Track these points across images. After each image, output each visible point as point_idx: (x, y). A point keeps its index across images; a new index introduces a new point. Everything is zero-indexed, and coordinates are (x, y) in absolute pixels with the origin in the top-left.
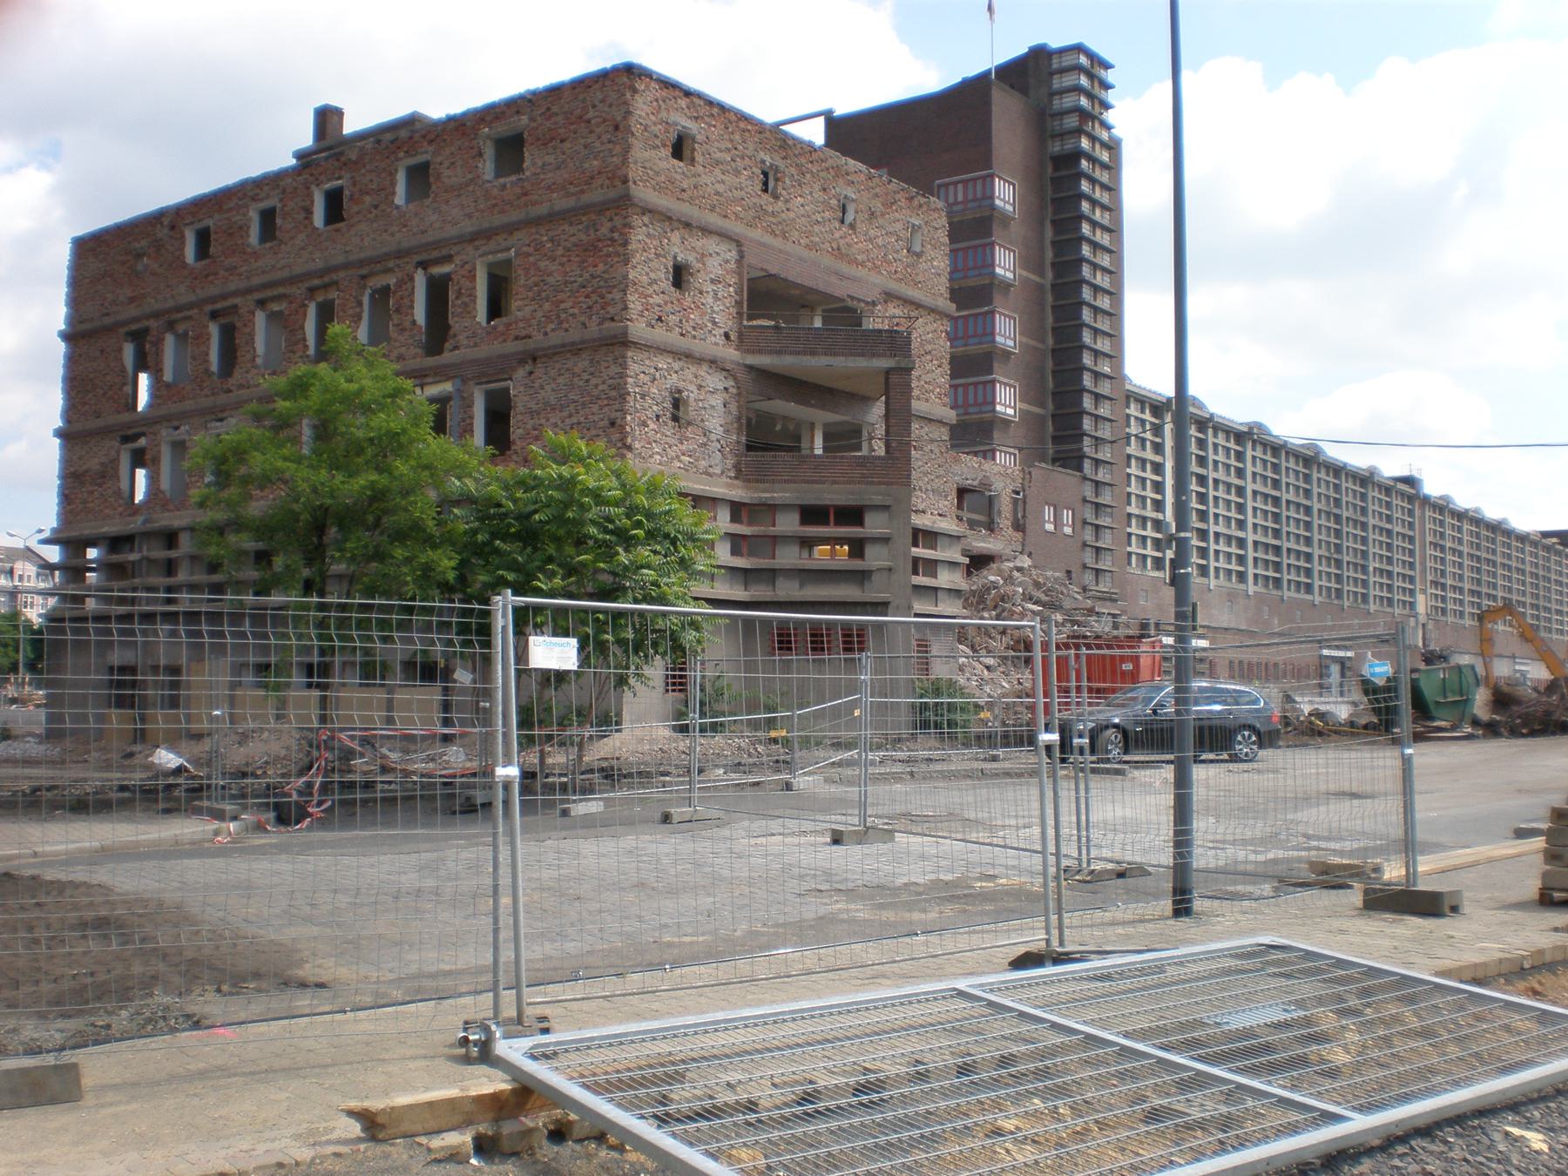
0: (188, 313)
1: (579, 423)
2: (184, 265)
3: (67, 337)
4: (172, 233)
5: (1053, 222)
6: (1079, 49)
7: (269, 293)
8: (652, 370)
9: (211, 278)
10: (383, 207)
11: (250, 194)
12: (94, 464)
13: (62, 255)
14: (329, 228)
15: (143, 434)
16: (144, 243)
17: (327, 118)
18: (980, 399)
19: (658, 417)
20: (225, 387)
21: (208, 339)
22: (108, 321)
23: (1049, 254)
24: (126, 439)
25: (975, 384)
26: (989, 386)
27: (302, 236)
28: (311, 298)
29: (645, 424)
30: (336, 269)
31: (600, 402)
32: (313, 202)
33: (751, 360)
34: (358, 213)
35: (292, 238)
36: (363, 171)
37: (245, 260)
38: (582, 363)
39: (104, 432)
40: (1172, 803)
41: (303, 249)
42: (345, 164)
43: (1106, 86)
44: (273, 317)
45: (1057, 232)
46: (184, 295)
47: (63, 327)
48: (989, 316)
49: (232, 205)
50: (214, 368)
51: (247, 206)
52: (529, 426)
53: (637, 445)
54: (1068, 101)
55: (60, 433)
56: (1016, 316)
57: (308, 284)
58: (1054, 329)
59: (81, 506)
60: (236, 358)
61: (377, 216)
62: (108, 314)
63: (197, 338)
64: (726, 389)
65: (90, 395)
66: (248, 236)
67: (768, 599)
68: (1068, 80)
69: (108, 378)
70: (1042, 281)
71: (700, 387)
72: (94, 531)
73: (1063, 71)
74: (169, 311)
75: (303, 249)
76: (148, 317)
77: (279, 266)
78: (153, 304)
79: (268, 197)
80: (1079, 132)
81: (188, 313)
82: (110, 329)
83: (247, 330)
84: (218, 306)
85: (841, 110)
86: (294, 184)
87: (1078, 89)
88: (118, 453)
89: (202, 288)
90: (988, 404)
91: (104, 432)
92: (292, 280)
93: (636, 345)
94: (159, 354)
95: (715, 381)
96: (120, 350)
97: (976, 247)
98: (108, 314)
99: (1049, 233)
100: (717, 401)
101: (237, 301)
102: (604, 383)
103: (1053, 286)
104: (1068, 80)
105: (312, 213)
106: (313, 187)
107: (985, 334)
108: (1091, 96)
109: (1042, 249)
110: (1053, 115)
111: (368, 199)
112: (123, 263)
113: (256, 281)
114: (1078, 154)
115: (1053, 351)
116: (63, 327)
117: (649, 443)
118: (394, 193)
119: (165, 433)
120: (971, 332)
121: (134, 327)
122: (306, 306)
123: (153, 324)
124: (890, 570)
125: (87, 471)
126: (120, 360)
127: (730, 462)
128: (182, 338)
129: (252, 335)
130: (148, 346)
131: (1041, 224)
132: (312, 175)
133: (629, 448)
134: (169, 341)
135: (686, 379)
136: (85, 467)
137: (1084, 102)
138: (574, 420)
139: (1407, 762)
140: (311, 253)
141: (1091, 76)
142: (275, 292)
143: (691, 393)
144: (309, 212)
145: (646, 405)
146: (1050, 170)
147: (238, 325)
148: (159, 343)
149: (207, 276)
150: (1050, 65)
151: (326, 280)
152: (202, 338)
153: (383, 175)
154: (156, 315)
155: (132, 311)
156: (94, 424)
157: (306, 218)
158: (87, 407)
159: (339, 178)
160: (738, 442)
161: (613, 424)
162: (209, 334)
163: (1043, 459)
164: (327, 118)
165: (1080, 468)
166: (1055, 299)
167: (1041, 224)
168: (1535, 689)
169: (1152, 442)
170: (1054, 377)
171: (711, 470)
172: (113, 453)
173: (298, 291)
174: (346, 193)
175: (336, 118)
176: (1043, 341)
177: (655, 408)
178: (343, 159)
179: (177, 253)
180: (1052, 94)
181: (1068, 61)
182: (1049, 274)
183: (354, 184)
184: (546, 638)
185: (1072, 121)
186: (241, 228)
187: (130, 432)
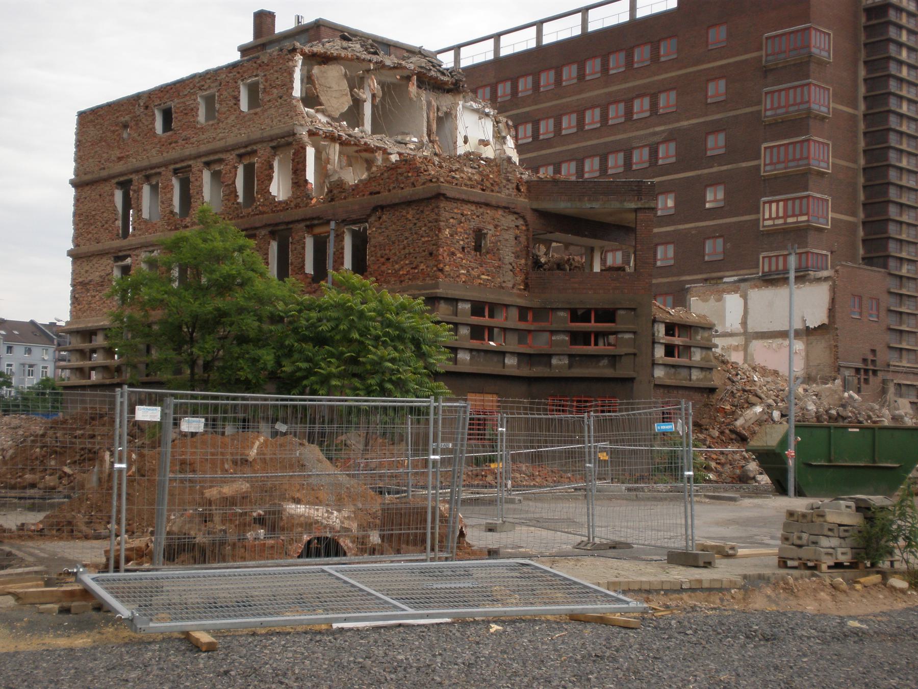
0: (158, 170)
1: (410, 254)
2: (155, 135)
3: (75, 184)
4: (146, 112)
5: (865, 63)
7: (212, 158)
8: (459, 216)
9: (173, 145)
10: (285, 97)
11: (198, 85)
12: (95, 276)
13: (74, 119)
14: (252, 111)
15: (129, 256)
16: (127, 118)
17: (263, 20)
19: (463, 248)
20: (184, 223)
21: (172, 189)
22: (104, 174)
23: (862, 90)
24: (118, 259)
25: (794, 199)
27: (233, 117)
28: (240, 162)
29: (453, 254)
30: (256, 142)
31: (423, 239)
32: (239, 92)
33: (536, 205)
34: (269, 101)
35: (227, 118)
36: (272, 71)
37: (196, 134)
38: (411, 214)
39: (102, 254)
41: (233, 126)
42: (260, 66)
44: (216, 175)
45: (869, 71)
46: (154, 156)
47: (73, 177)
48: (805, 144)
49: (186, 93)
50: (177, 210)
51: (195, 94)
52: (379, 255)
53: (447, 268)
55: (70, 254)
56: (830, 143)
57: (238, 152)
58: (865, 151)
59: (87, 306)
60: (191, 203)
61: (281, 104)
62: (104, 169)
63: (164, 188)
64: (517, 226)
65: (93, 227)
66: (197, 116)
67: (546, 375)
69: (105, 215)
70: (856, 112)
71: (496, 226)
72: (96, 324)
74: (146, 169)
75: (233, 126)
76: (131, 173)
77: (218, 138)
78: (134, 163)
79: (209, 87)
81: (158, 170)
82: (106, 180)
83: (198, 184)
84: (178, 166)
86: (227, 79)
88: (112, 268)
89: (168, 152)
91: (102, 254)
92: (226, 150)
93: (447, 198)
94: (139, 198)
95: (509, 221)
96: (113, 195)
97: (795, 87)
98: (104, 169)
99: (862, 73)
100: (510, 236)
101: (190, 163)
102: (425, 225)
103: (865, 116)
105: (239, 100)
106: (240, 82)
109: (856, 86)
111: (275, 91)
112: (114, 132)
113: (203, 148)
115: (864, 169)
116: (73, 177)
117: (457, 267)
118: (292, 88)
119: (144, 255)
120: (791, 157)
121: (122, 179)
122: (236, 168)
123: (134, 177)
124: (635, 354)
125: (91, 281)
126: (112, 202)
127: (519, 278)
128: (154, 189)
129: (201, 186)
130: (131, 193)
131: (855, 63)
132: (239, 73)
133: (441, 270)
134: (146, 189)
135: (488, 220)
136: (90, 278)
138: (407, 251)
140: (239, 129)
142: (216, 157)
143: (490, 230)
144: (237, 99)
145: (455, 241)
147: (192, 179)
148: (139, 191)
149: (170, 144)
151: (249, 149)
152: (169, 188)
153: (285, 74)
154: (137, 171)
155: (119, 167)
156: (95, 247)
157: (235, 104)
158: (90, 236)
159: (256, 76)
160: (526, 264)
161: (431, 254)
162: (172, 185)
163: (853, 259)
164: (263, 20)
165: (885, 266)
166: (867, 126)
167: (855, 63)
170: (864, 191)
171: (504, 285)
172: (109, 268)
173: (231, 157)
174: (261, 86)
175: (269, 20)
176: (855, 161)
177: (461, 243)
178: (259, 62)
179: (151, 126)
182: (862, 107)
183: (266, 81)
184: (144, 407)
186: (192, 109)
187: (120, 254)
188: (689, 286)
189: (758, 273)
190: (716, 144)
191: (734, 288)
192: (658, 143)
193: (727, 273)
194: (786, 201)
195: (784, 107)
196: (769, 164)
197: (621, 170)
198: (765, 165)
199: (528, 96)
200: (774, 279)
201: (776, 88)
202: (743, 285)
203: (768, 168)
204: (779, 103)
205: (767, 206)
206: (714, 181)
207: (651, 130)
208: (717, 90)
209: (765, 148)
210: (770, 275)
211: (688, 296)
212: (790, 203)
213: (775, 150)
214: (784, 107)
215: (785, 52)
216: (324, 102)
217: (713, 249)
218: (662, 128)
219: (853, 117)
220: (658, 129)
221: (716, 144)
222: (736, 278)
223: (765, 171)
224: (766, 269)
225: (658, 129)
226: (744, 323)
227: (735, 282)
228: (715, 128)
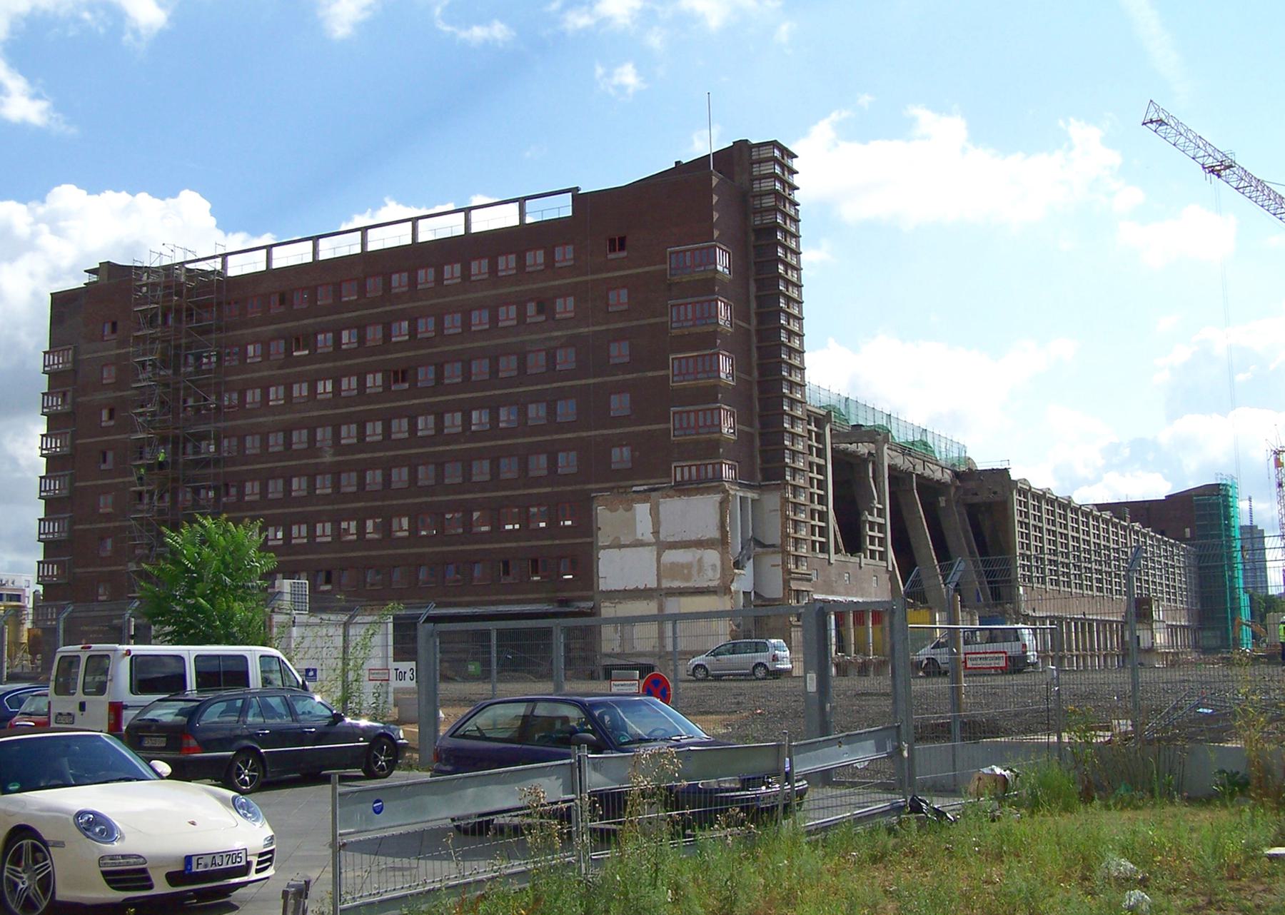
5: (756, 280)
6: (775, 144)
18: (709, 422)
23: (753, 305)
25: (704, 411)
26: (716, 412)
40: (684, 539)
43: (793, 172)
54: (766, 185)
68: (766, 169)
73: (760, 162)
80: (775, 210)
85: (588, 186)
87: (774, 176)
90: (711, 264)
104: (766, 169)
107: (710, 317)
108: (783, 182)
109: (748, 301)
110: (754, 197)
114: (777, 227)
137: (778, 186)
139: (778, 565)
141: (783, 166)
146: (753, 238)
150: (751, 156)
168: (24, 619)
169: (815, 432)
180: (753, 179)
181: (765, 153)
185: (769, 201)
188: (595, 495)
189: (671, 483)
190: (619, 352)
191: (644, 496)
192: (557, 348)
193: (637, 482)
194: (694, 304)
195: (691, 320)
196: (676, 322)
197: (514, 373)
198: (673, 376)
199: (404, 293)
200: (687, 489)
201: (680, 301)
202: (653, 494)
203: (675, 379)
204: (689, 424)
205: (674, 310)
206: (620, 388)
207: (547, 335)
208: (620, 299)
209: (673, 359)
210: (683, 485)
211: (594, 506)
212: (698, 306)
213: (682, 308)
214: (691, 320)
215: (690, 267)
216: (426, 625)
217: (621, 456)
218: (559, 333)
219: (751, 435)
220: (556, 334)
221: (619, 352)
222: (646, 487)
223: (673, 382)
224: (679, 478)
225: (556, 334)
226: (656, 533)
227: (645, 491)
228: (620, 336)
